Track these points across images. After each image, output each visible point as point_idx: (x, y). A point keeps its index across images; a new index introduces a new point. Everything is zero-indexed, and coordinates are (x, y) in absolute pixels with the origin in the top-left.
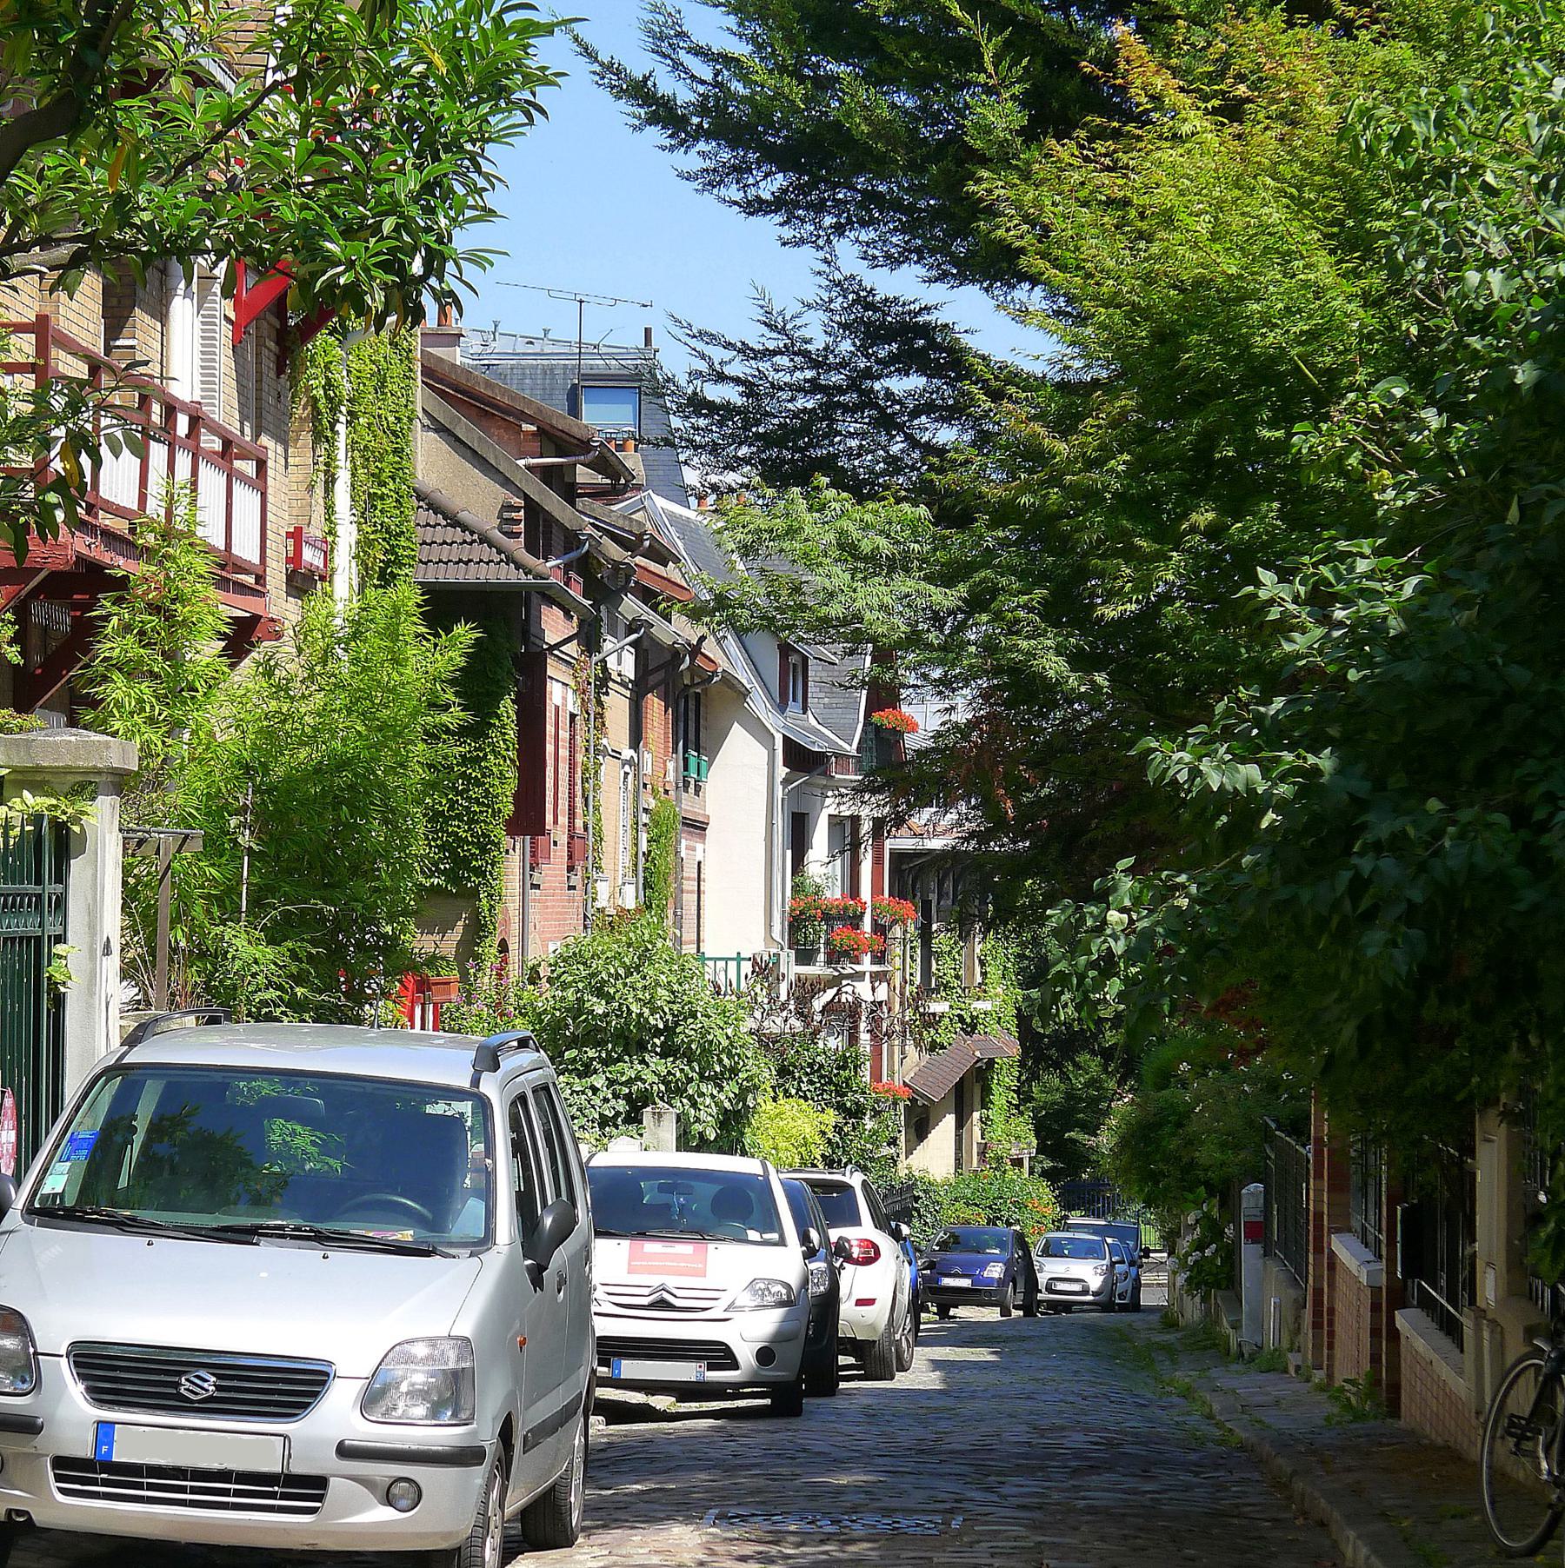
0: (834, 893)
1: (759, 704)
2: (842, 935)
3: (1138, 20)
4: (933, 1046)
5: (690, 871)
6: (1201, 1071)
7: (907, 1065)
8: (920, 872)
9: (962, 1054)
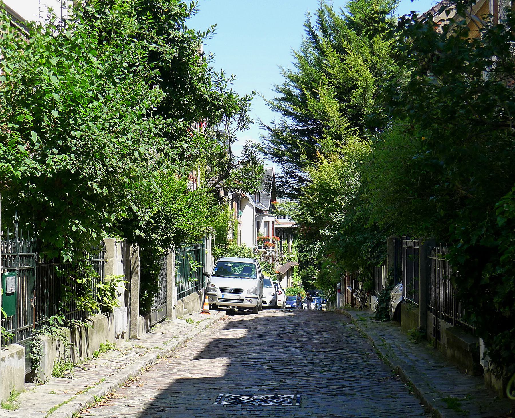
0: (265, 236)
1: (251, 201)
2: (267, 244)
3: (319, 262)
4: (283, 264)
5: (239, 232)
6: (331, 266)
7: (277, 267)
8: (280, 231)
9: (288, 265)
